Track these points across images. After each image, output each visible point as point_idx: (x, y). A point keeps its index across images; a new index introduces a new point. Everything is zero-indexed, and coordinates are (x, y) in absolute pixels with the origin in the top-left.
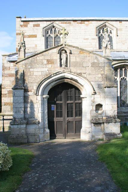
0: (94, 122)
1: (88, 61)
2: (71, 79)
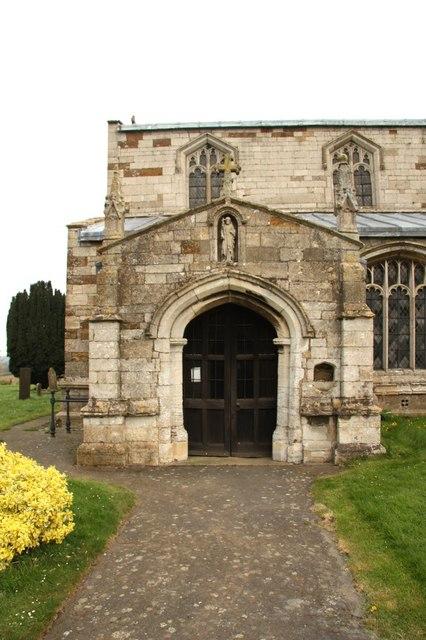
0: (309, 412)
2: (249, 294)
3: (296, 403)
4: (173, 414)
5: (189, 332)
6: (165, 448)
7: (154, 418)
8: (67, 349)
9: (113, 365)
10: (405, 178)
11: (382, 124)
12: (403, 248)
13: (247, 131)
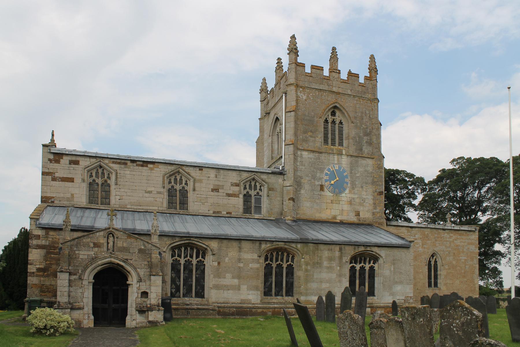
0: (139, 309)
1: (135, 247)
2: (118, 264)
3: (134, 306)
4: (88, 309)
5: (94, 278)
6: (85, 322)
7: (82, 310)
8: (28, 282)
9: (67, 289)
10: (205, 196)
11: (196, 165)
12: (190, 241)
13: (123, 161)
